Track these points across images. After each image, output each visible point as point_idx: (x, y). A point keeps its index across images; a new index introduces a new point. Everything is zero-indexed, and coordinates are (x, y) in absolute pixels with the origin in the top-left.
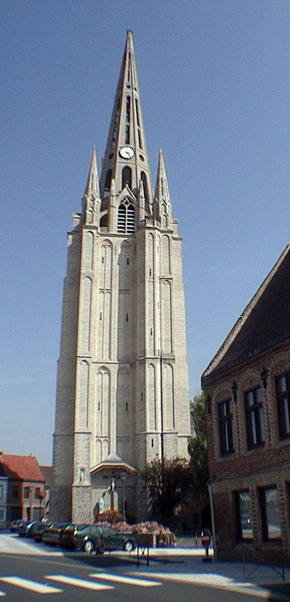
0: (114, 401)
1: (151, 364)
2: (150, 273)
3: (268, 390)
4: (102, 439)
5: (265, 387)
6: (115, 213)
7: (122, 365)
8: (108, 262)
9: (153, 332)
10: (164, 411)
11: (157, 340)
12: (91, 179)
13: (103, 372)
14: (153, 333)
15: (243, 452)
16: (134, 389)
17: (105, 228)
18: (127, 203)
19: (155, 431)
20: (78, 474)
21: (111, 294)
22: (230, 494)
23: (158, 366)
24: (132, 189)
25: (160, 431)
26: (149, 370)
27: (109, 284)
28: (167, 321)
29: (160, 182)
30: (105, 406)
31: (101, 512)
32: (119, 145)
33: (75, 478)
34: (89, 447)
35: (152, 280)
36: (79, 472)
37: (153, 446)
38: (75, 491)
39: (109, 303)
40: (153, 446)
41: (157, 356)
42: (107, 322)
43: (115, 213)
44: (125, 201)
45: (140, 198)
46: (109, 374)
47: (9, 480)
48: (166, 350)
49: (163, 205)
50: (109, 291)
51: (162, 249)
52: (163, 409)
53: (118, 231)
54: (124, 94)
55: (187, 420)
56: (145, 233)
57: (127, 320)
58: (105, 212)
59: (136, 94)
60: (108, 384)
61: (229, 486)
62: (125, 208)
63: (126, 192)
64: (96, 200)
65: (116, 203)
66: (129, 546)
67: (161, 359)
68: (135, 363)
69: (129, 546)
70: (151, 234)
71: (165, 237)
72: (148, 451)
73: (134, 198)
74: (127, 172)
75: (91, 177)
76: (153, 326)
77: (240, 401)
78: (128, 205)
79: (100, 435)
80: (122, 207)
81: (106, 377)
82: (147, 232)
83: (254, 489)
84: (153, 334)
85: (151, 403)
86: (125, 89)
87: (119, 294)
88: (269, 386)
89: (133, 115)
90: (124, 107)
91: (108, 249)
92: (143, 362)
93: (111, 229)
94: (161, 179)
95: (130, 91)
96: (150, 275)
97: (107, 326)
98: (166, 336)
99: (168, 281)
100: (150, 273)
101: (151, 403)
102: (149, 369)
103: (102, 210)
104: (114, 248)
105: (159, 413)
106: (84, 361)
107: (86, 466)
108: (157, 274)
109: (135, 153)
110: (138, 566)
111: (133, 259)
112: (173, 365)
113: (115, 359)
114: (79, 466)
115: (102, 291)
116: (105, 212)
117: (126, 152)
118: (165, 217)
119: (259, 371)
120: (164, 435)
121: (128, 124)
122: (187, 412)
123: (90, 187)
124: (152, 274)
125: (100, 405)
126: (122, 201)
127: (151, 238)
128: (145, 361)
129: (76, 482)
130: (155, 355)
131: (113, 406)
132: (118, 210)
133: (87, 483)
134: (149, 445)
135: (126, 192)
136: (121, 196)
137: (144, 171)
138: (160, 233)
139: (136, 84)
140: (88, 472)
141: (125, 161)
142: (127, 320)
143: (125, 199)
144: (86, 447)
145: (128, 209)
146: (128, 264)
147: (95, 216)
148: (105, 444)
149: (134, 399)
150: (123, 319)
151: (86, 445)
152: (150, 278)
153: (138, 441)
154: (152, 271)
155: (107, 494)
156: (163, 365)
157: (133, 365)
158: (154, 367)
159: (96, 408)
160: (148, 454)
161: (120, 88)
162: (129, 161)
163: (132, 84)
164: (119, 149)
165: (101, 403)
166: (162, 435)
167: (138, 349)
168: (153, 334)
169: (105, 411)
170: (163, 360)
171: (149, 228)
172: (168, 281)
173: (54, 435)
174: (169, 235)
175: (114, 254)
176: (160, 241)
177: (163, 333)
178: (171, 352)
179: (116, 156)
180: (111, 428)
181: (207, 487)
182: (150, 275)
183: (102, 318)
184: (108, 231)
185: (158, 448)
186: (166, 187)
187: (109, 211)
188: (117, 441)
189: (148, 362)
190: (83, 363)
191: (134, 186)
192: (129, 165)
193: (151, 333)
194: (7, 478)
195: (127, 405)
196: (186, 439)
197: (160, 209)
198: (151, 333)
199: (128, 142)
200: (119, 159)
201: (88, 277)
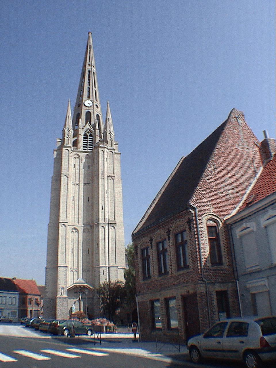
0: (81, 248)
1: (103, 226)
3: (171, 242)
4: (74, 270)
5: (169, 240)
6: (81, 138)
7: (85, 227)
8: (77, 167)
9: (103, 208)
11: (106, 213)
13: (74, 231)
14: (103, 208)
15: (156, 278)
16: (92, 241)
17: (76, 147)
18: (88, 133)
20: (60, 290)
21: (79, 185)
22: (215, 297)
23: (107, 227)
25: (108, 266)
27: (78, 180)
28: (111, 201)
29: (108, 120)
30: (75, 251)
31: (73, 313)
32: (84, 99)
33: (58, 293)
35: (103, 178)
36: (61, 289)
37: (103, 274)
38: (58, 300)
39: (78, 191)
40: (103, 274)
41: (106, 222)
42: (77, 202)
43: (81, 138)
44: (87, 132)
45: (96, 130)
46: (78, 232)
48: (111, 218)
49: (109, 134)
50: (78, 184)
52: (110, 252)
53: (83, 149)
54: (87, 69)
55: (124, 259)
56: (99, 150)
57: (88, 201)
58: (76, 138)
59: (94, 69)
60: (77, 238)
61: (148, 298)
62: (87, 136)
63: (88, 126)
64: (71, 131)
65: (82, 133)
66: (89, 333)
67: (108, 224)
68: (93, 226)
69: (89, 333)
70: (102, 150)
72: (100, 277)
73: (92, 129)
74: (88, 114)
77: (154, 248)
78: (89, 134)
79: (72, 268)
80: (85, 135)
81: (76, 234)
82: (100, 149)
83: (163, 299)
84: (103, 209)
85: (102, 249)
86: (87, 66)
87: (84, 185)
88: (171, 239)
90: (87, 77)
91: (78, 160)
92: (98, 225)
93: (79, 148)
94: (108, 119)
95: (90, 67)
96: (102, 174)
99: (112, 178)
102: (101, 230)
103: (74, 137)
104: (81, 159)
105: (107, 255)
106: (63, 224)
107: (64, 286)
108: (106, 174)
109: (93, 104)
110: (95, 344)
111: (92, 165)
112: (115, 227)
113: (81, 224)
114: (60, 286)
116: (76, 138)
117: (88, 103)
118: (110, 141)
119: (166, 230)
120: (110, 268)
121: (89, 86)
124: (103, 174)
126: (86, 131)
128: (99, 225)
129: (59, 295)
130: (104, 221)
131: (80, 251)
132: (83, 137)
133: (65, 296)
134: (101, 274)
135: (88, 126)
136: (85, 129)
138: (107, 150)
139: (93, 64)
140: (66, 289)
141: (87, 108)
142: (88, 201)
143: (87, 130)
145: (89, 136)
146: (89, 168)
147: (70, 141)
148: (76, 273)
149: (93, 248)
150: (86, 200)
151: (65, 274)
152: (102, 176)
153: (95, 271)
154: (103, 172)
155: (77, 302)
156: (109, 227)
157: (92, 227)
158: (104, 228)
159: (70, 252)
160: (101, 279)
161: (85, 65)
162: (89, 108)
164: (84, 101)
165: (73, 249)
166: (109, 267)
167: (95, 218)
168: (103, 209)
171: (101, 147)
172: (112, 178)
173: (46, 268)
176: (108, 155)
179: (82, 105)
181: (135, 298)
182: (102, 174)
183: (74, 199)
184: (77, 149)
186: (111, 123)
187: (78, 137)
189: (101, 225)
191: (92, 123)
192: (90, 111)
193: (103, 209)
195: (88, 250)
198: (103, 209)
200: (83, 107)
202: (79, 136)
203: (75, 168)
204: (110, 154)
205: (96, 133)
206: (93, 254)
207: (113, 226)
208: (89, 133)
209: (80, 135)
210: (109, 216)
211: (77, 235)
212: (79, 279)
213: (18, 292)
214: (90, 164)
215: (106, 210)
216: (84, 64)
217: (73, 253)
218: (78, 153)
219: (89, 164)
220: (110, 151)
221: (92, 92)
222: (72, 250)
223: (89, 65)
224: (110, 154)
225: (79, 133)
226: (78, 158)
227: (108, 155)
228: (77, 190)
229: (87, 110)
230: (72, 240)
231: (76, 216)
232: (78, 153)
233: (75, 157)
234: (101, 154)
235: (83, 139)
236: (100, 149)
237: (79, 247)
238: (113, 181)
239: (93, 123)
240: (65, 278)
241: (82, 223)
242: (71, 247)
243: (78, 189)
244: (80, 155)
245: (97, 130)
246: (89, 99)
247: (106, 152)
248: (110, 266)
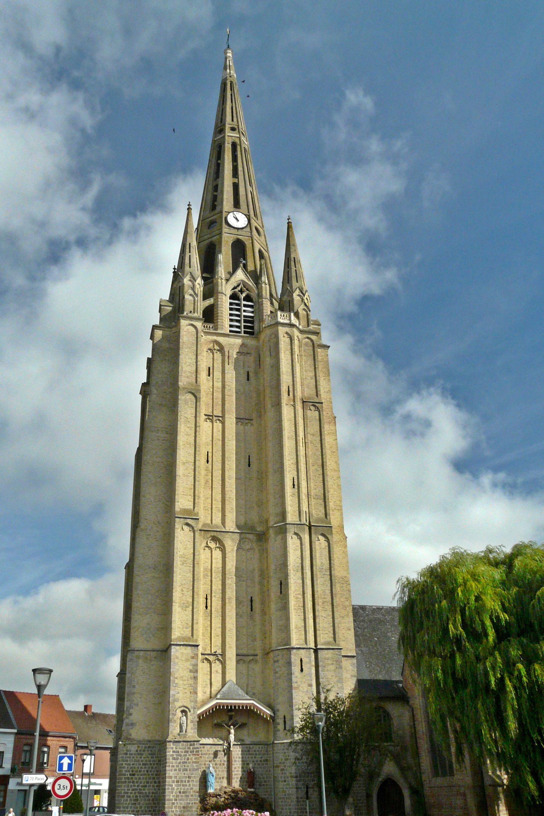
0: (231, 593)
1: (296, 534)
2: (289, 392)
4: (211, 658)
6: (225, 303)
7: (243, 535)
8: (218, 374)
9: (296, 483)
10: (318, 611)
11: (304, 497)
12: (187, 250)
14: (296, 485)
16: (263, 574)
17: (211, 325)
19: (305, 646)
21: (223, 423)
23: (306, 538)
24: (249, 271)
25: (312, 645)
26: (294, 543)
27: (220, 408)
28: (316, 467)
29: (293, 263)
30: (216, 603)
31: (211, 791)
34: (197, 671)
35: (292, 403)
36: (179, 714)
37: (302, 670)
38: (170, 750)
39: (220, 437)
40: (302, 670)
41: (304, 521)
42: (218, 466)
43: (225, 303)
44: (239, 288)
45: (263, 285)
46: (223, 549)
47: (16, 734)
48: (318, 512)
49: (299, 295)
50: (221, 419)
51: (304, 358)
52: (317, 607)
53: (231, 331)
55: (349, 630)
56: (277, 331)
57: (249, 465)
58: (210, 301)
59: (245, 142)
60: (220, 565)
62: (238, 299)
64: (197, 282)
67: (310, 527)
70: (287, 333)
71: (307, 340)
72: (294, 679)
73: (251, 283)
75: (188, 246)
76: (296, 474)
78: (244, 295)
80: (234, 296)
81: (217, 554)
82: (282, 330)
84: (296, 487)
85: (297, 598)
86: (228, 133)
87: (237, 423)
89: (243, 168)
90: (228, 156)
91: (218, 356)
92: (282, 531)
93: (219, 326)
94: (293, 259)
95: (235, 134)
96: (289, 395)
97: (218, 474)
98: (317, 490)
100: (289, 392)
101: (297, 598)
102: (292, 543)
103: (205, 298)
104: (227, 354)
105: (310, 615)
106: (187, 524)
108: (299, 394)
111: (256, 373)
112: (329, 537)
113: (231, 525)
114: (178, 704)
115: (209, 419)
116: (210, 301)
118: (305, 313)
120: (320, 653)
121: (236, 180)
122: (348, 615)
123: (187, 261)
124: (291, 394)
125: (209, 601)
126: (235, 288)
127: (288, 340)
128: (286, 529)
129: (174, 730)
130: (300, 520)
131: (230, 602)
133: (192, 733)
134: (296, 669)
137: (262, 249)
138: (300, 336)
139: (243, 127)
140: (193, 716)
141: (235, 231)
143: (238, 286)
144: (191, 671)
145: (244, 300)
146: (248, 380)
148: (217, 667)
150: (244, 462)
151: (191, 668)
152: (289, 400)
153: (275, 662)
154: (291, 389)
155: (221, 755)
156: (313, 536)
157: (262, 537)
158: (300, 539)
159: (203, 606)
160: (294, 685)
161: (220, 130)
162: (240, 232)
163: (238, 126)
164: (224, 214)
165: (209, 598)
166: (316, 651)
167: (272, 510)
168: (296, 487)
169: (217, 611)
170: (312, 527)
171: (283, 324)
174: (314, 337)
175: (226, 364)
176: (300, 347)
177: (312, 485)
178: (323, 516)
179: (221, 225)
180: (228, 639)
182: (289, 395)
183: (210, 460)
184: (216, 329)
185: (310, 674)
187: (216, 300)
188: (238, 662)
189: (291, 530)
190: (185, 527)
191: (251, 267)
192: (240, 237)
193: (294, 485)
194: (15, 731)
195: (252, 601)
196: (64, 770)
197: (295, 302)
198: (294, 485)
199: (237, 205)
200: (225, 229)
201: (193, 394)
202: (220, 296)
203: (210, 378)
204: (306, 344)
205: (264, 293)
206: (264, 613)
207: (323, 535)
208: (239, 291)
209: (222, 293)
210: (313, 507)
211: (220, 555)
212: (226, 686)
213: (14, 728)
214: (251, 370)
215: (304, 490)
216: (216, 126)
217: (209, 608)
218: (309, 336)
219: (247, 369)
220: (305, 336)
221: (244, 193)
222: (207, 599)
223: (233, 129)
224: (306, 344)
225: (220, 288)
226: (218, 350)
227: (301, 346)
228: (218, 435)
229: (236, 237)
230: (205, 569)
231: (218, 505)
232: (309, 336)
233: (212, 348)
234: (284, 341)
235: (228, 306)
236: (280, 328)
237: (228, 590)
238: (317, 412)
239: (253, 269)
240: (191, 682)
241: (234, 526)
242: (204, 591)
243: (220, 433)
244: (223, 344)
245: (266, 284)
246: (237, 210)
247: (296, 338)
248: (318, 647)
